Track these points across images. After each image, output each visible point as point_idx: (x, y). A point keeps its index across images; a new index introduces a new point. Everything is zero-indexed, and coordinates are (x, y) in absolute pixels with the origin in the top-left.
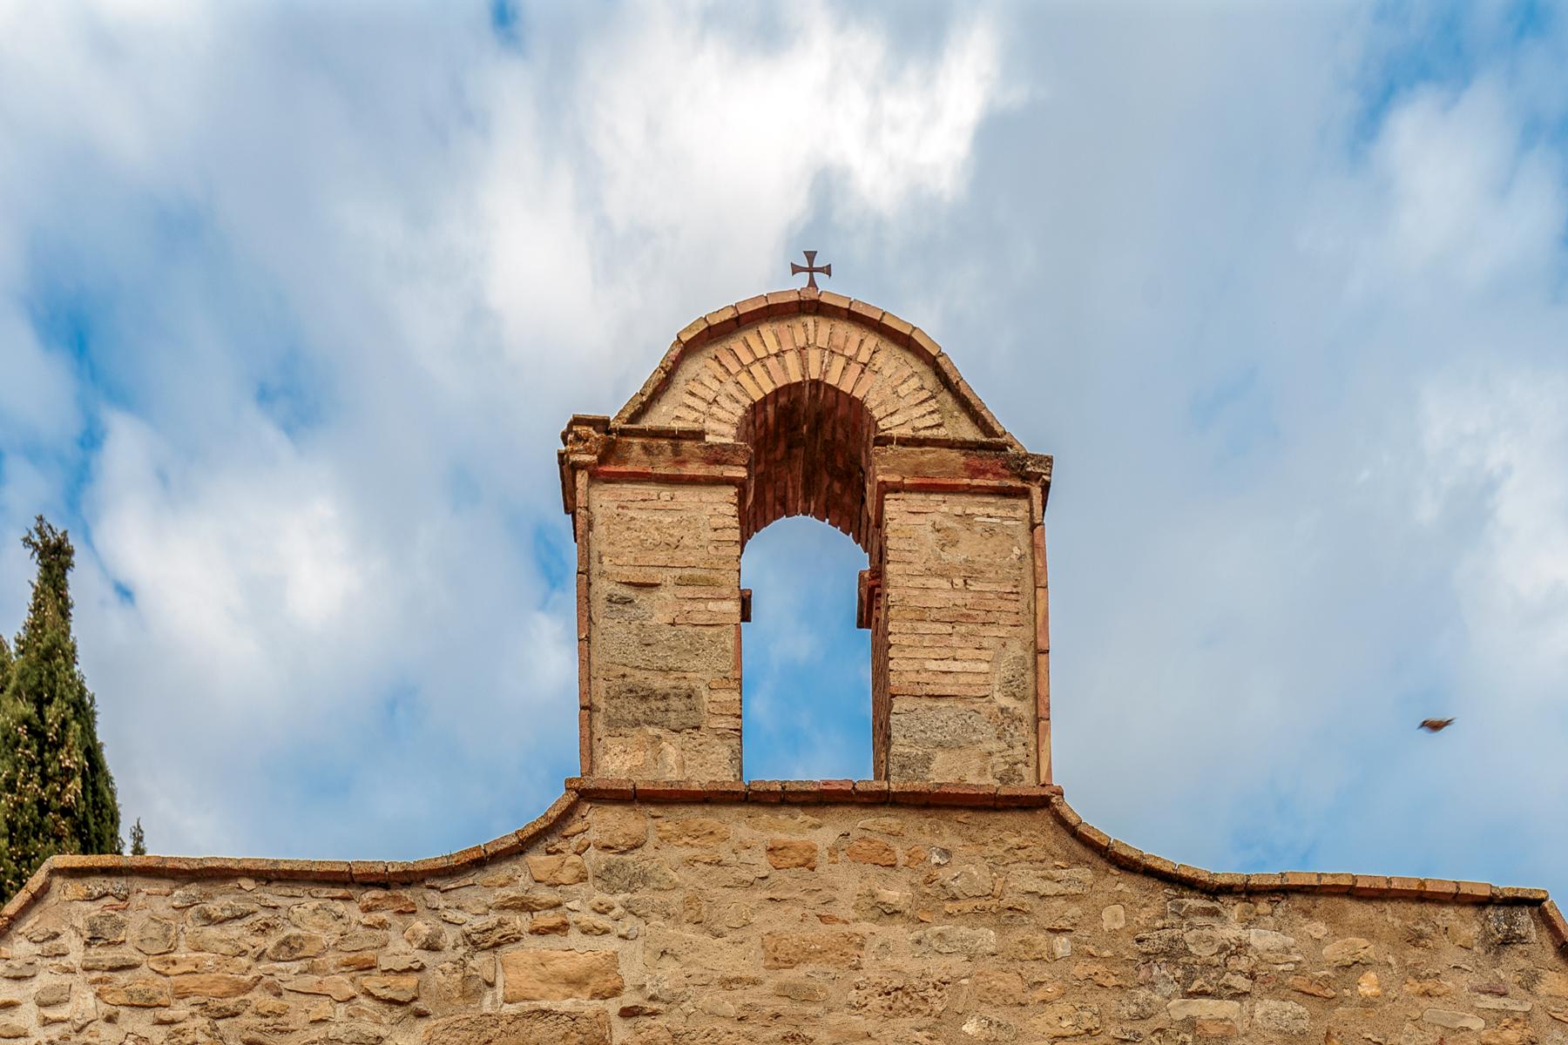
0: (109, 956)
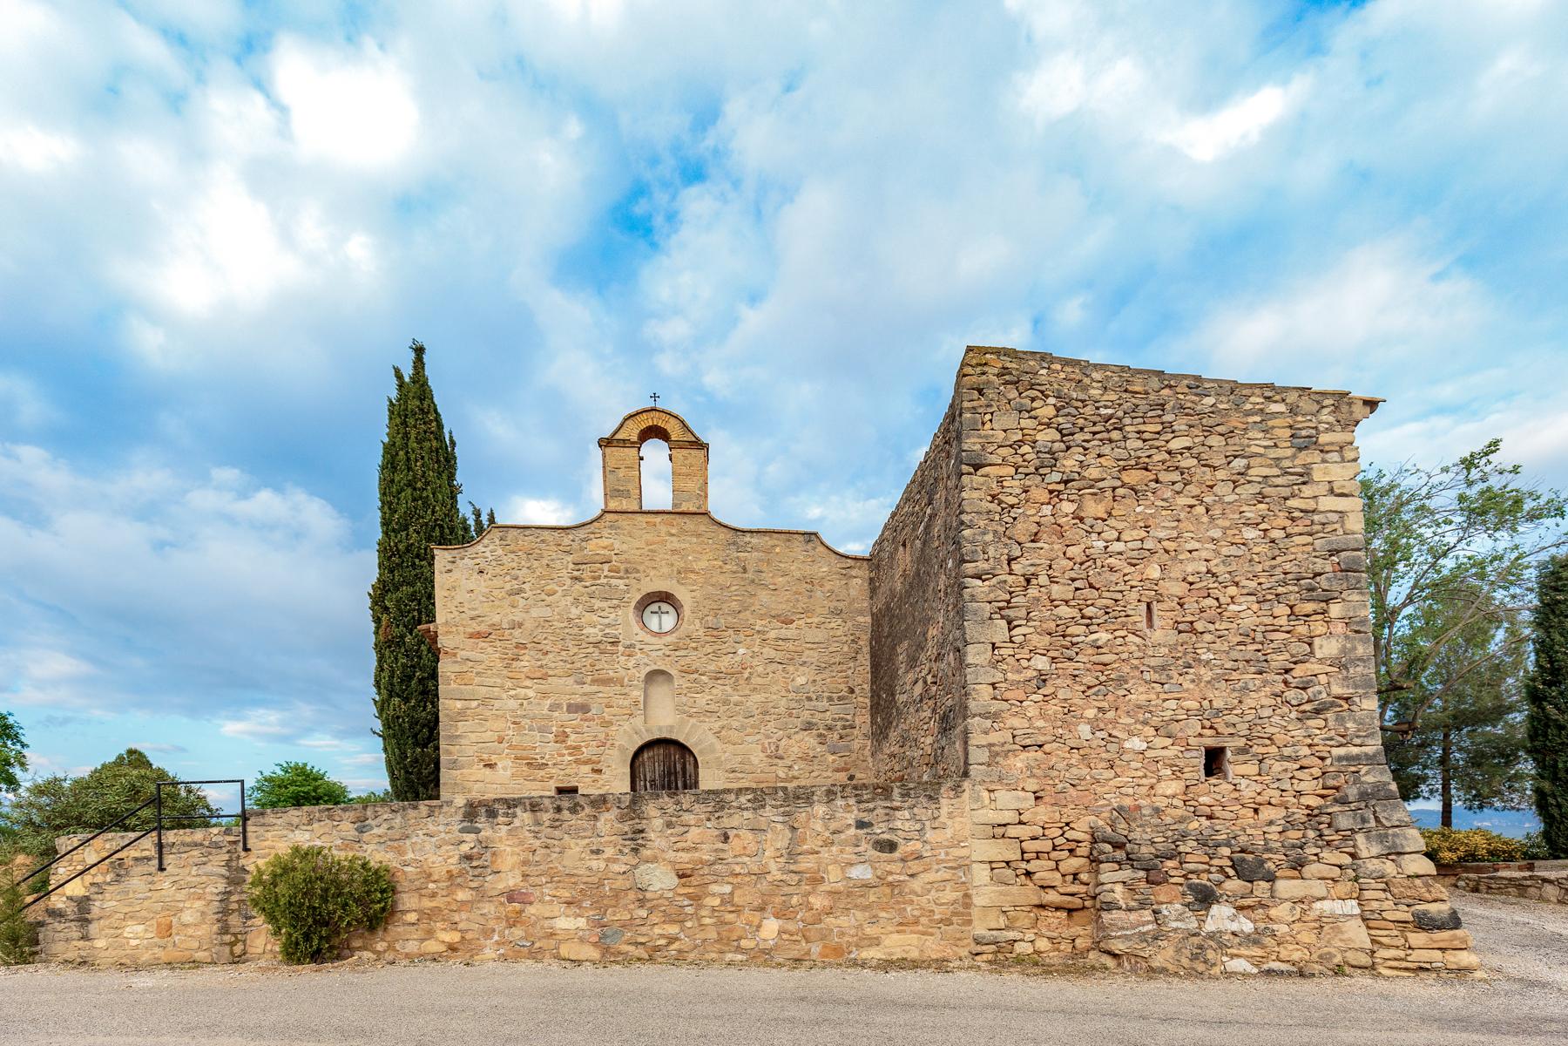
0: (505, 543)
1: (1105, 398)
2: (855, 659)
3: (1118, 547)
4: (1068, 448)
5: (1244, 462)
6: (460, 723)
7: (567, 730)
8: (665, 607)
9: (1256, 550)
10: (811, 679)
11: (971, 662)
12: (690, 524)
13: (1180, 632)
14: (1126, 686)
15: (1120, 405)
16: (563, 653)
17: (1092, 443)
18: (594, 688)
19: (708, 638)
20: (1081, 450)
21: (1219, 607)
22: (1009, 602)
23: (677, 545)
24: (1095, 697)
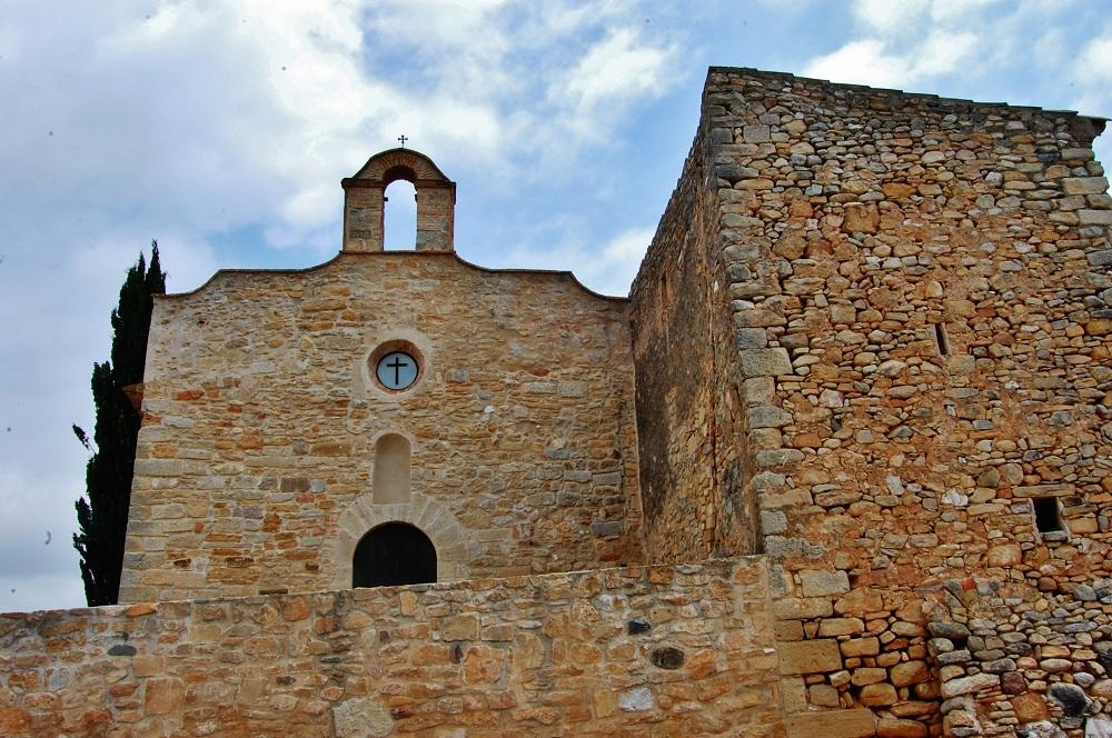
0: (231, 289)
1: (851, 114)
2: (619, 416)
3: (893, 263)
4: (824, 161)
5: (998, 176)
6: (154, 507)
7: (279, 514)
8: (403, 359)
9: (1032, 264)
10: (570, 441)
11: (752, 400)
12: (434, 267)
13: (977, 357)
14: (930, 425)
15: (867, 121)
16: (283, 416)
17: (848, 156)
18: (318, 459)
19: (451, 395)
20: (838, 163)
21: (1011, 328)
22: (786, 326)
23: (419, 288)
24: (899, 440)
